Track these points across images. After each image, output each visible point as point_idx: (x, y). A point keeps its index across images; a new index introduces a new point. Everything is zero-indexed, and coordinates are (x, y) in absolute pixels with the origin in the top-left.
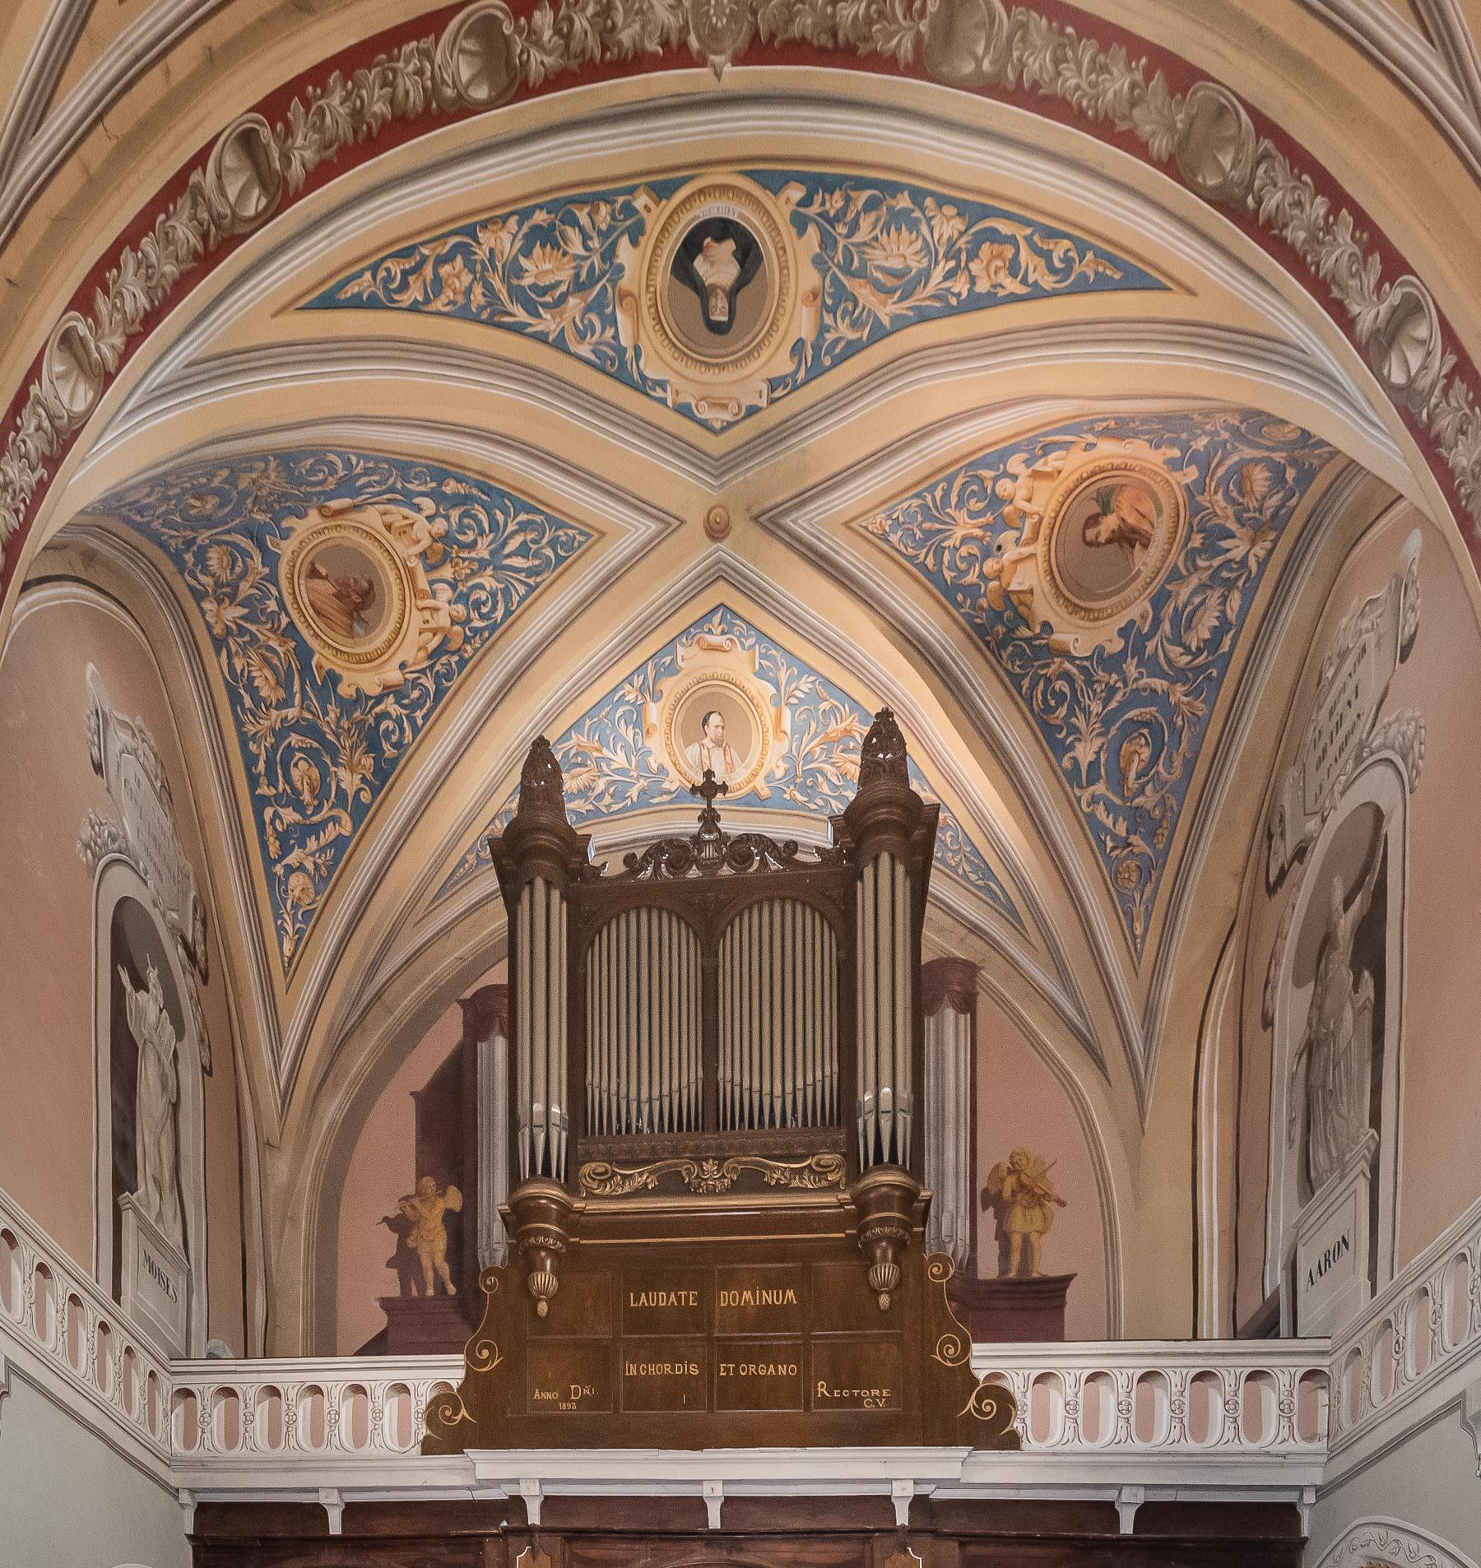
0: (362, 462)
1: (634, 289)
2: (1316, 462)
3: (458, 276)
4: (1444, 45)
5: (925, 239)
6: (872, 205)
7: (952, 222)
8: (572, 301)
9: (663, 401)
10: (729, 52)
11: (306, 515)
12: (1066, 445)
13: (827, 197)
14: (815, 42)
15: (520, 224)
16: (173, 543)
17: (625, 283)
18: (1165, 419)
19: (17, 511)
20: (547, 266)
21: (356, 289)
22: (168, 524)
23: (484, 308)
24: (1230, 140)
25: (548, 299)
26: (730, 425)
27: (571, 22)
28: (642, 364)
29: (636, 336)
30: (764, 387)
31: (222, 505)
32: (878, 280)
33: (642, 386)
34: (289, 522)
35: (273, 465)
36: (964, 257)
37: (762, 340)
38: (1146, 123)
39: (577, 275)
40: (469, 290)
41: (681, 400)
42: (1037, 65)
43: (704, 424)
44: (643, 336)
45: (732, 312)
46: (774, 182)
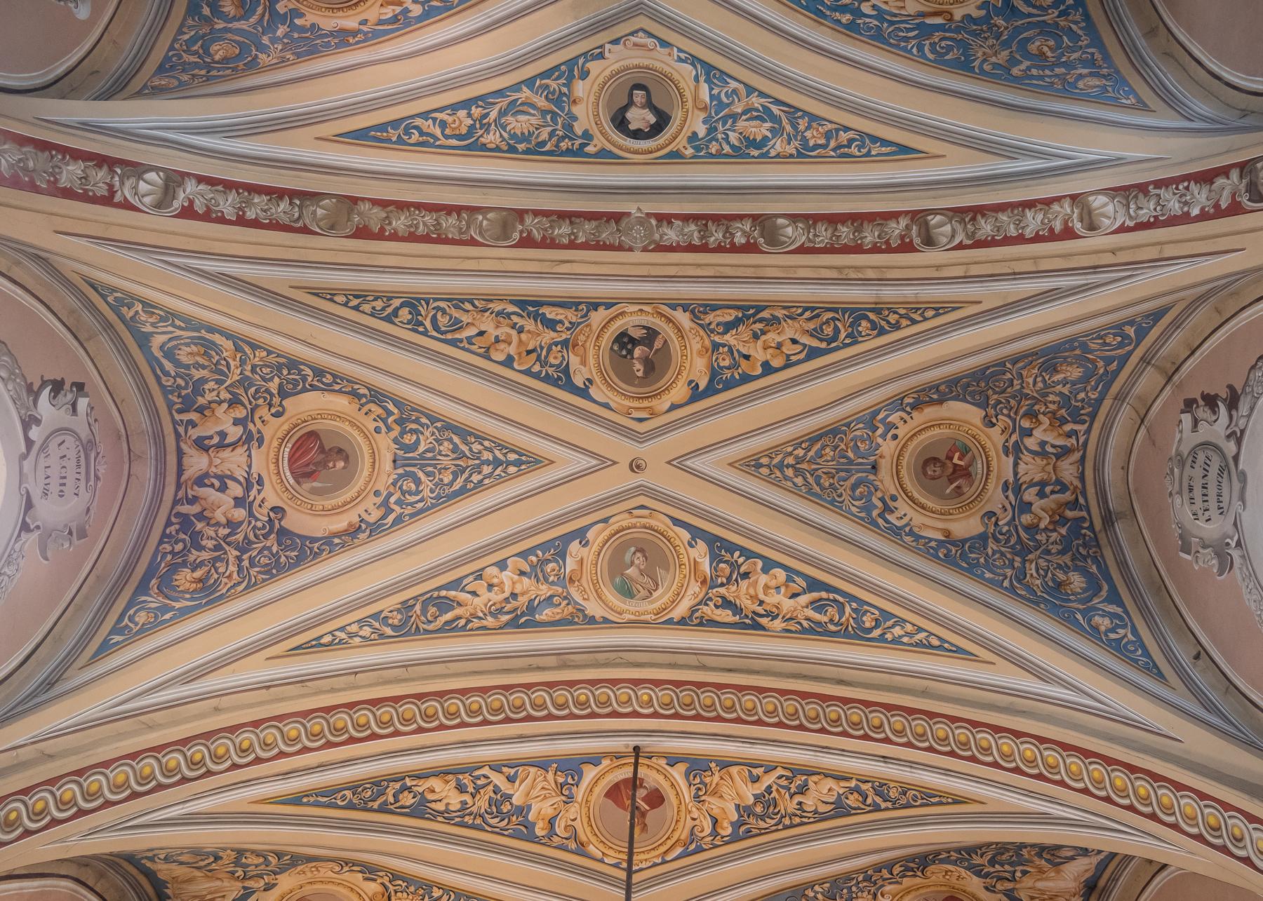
0: (909, 48)
1: (696, 112)
2: (190, 22)
3: (814, 137)
4: (213, 276)
5: (505, 131)
6: (544, 143)
7: (489, 141)
8: (739, 110)
9: (680, 50)
10: (632, 217)
11: (964, 17)
12: (380, 22)
13: (570, 147)
14: (582, 219)
15: (768, 152)
16: (1078, 18)
17: (702, 115)
18: (312, 52)
19: (1187, 188)
20: (753, 130)
21: (883, 149)
22: (1074, 37)
23: (799, 117)
24: (321, 220)
25: (756, 114)
26: (632, 34)
27: (724, 236)
28: (694, 73)
29: (697, 88)
30: (607, 55)
31: (1028, 40)
32: (534, 110)
33: (694, 60)
34: (976, 14)
35: (976, 63)
36: (478, 126)
37: (609, 80)
38: (379, 213)
39: (734, 122)
40: (807, 128)
41: (666, 51)
42: (450, 221)
43: (651, 35)
44: (692, 88)
45: (631, 95)
46: (603, 154)
